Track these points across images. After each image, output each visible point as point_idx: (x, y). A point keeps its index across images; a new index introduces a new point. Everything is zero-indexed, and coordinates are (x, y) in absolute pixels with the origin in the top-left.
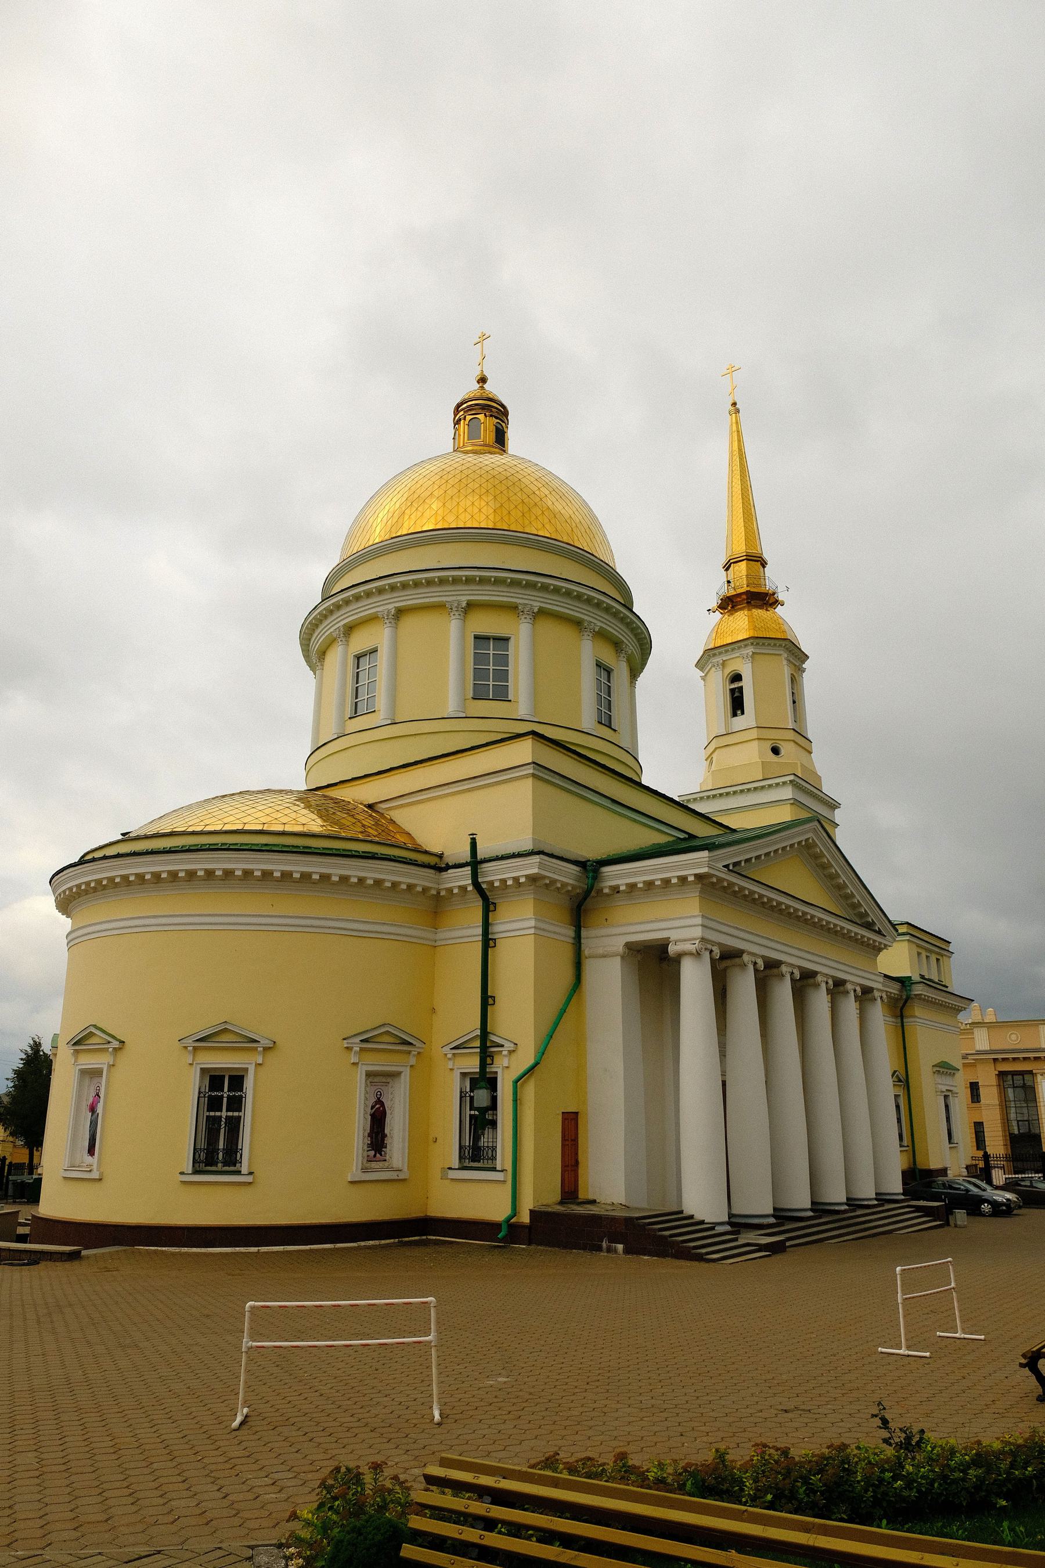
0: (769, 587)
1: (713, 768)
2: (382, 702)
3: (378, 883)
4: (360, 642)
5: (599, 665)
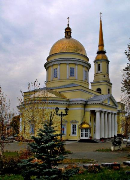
0: (104, 50)
1: (95, 78)
2: (58, 76)
3: (60, 103)
4: (55, 67)
5: (85, 71)
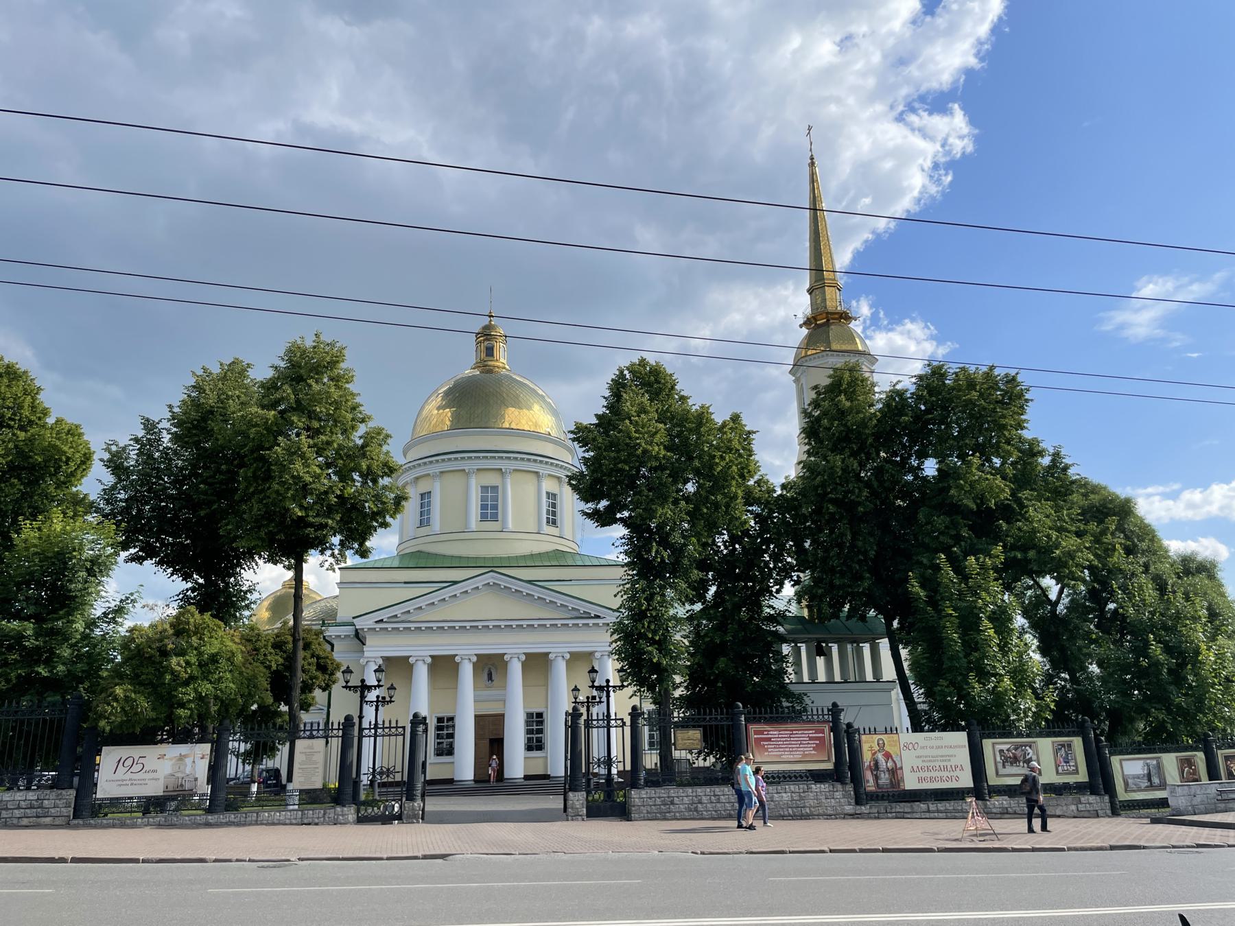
4: (423, 487)
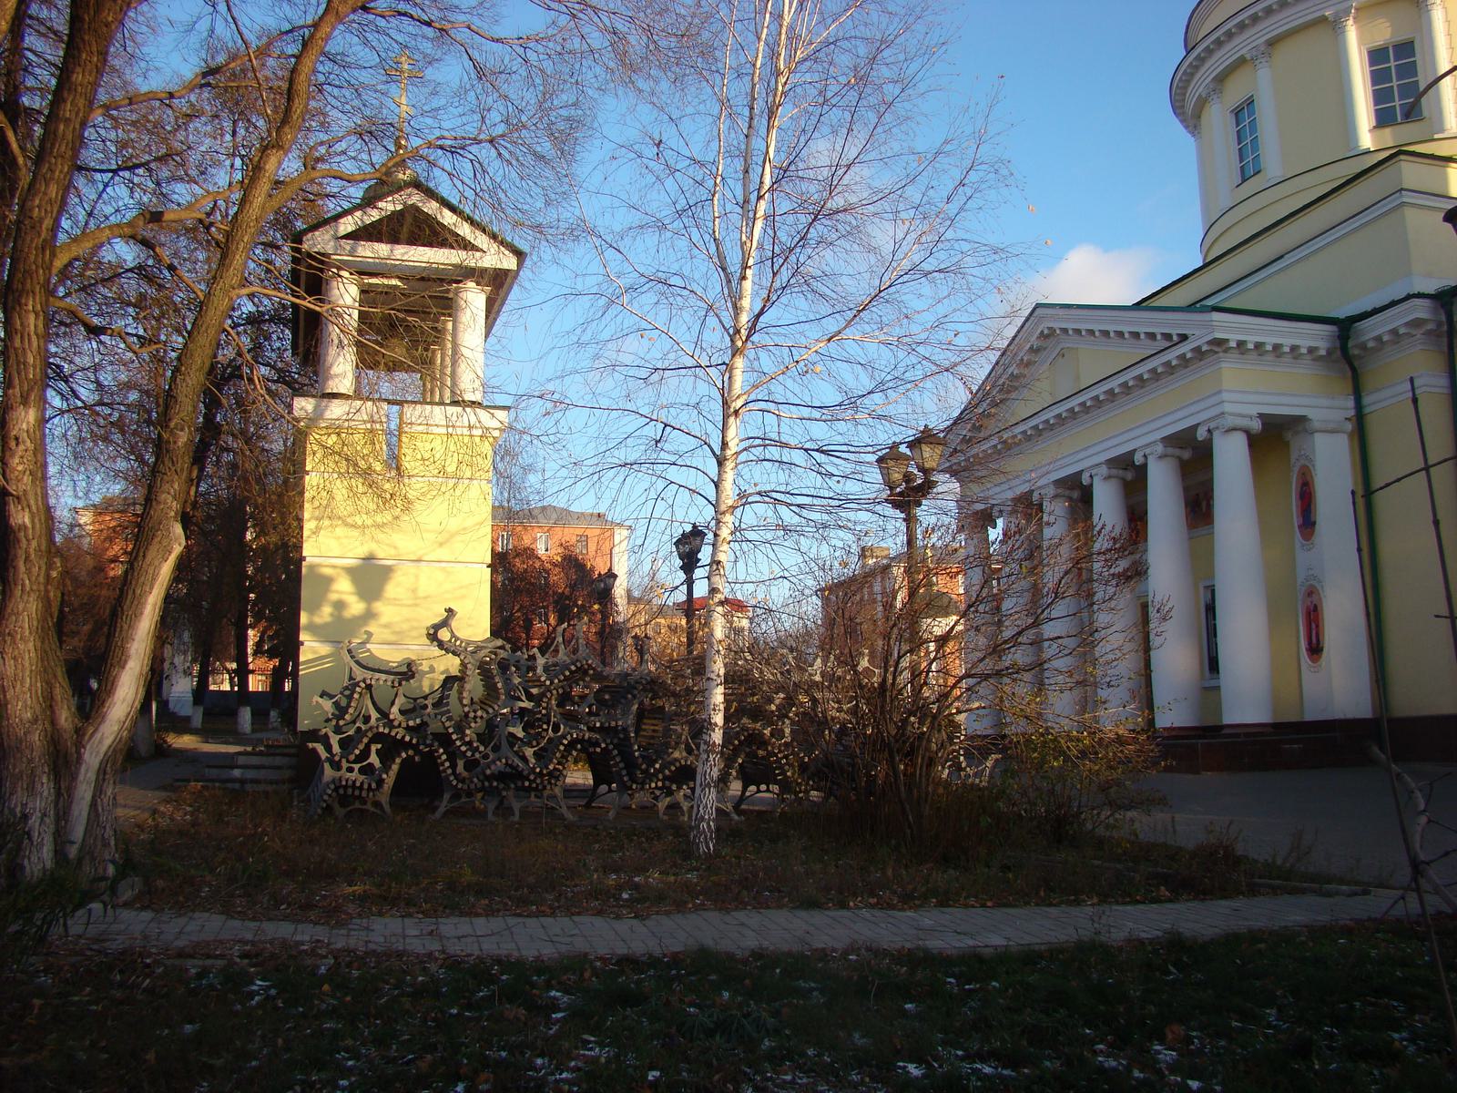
4: (1235, 92)
